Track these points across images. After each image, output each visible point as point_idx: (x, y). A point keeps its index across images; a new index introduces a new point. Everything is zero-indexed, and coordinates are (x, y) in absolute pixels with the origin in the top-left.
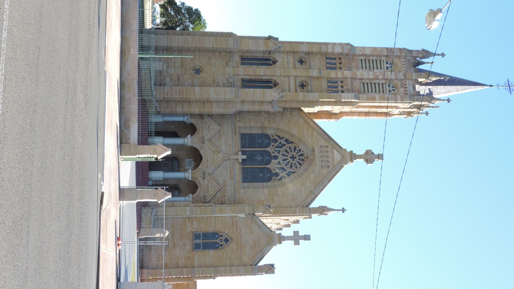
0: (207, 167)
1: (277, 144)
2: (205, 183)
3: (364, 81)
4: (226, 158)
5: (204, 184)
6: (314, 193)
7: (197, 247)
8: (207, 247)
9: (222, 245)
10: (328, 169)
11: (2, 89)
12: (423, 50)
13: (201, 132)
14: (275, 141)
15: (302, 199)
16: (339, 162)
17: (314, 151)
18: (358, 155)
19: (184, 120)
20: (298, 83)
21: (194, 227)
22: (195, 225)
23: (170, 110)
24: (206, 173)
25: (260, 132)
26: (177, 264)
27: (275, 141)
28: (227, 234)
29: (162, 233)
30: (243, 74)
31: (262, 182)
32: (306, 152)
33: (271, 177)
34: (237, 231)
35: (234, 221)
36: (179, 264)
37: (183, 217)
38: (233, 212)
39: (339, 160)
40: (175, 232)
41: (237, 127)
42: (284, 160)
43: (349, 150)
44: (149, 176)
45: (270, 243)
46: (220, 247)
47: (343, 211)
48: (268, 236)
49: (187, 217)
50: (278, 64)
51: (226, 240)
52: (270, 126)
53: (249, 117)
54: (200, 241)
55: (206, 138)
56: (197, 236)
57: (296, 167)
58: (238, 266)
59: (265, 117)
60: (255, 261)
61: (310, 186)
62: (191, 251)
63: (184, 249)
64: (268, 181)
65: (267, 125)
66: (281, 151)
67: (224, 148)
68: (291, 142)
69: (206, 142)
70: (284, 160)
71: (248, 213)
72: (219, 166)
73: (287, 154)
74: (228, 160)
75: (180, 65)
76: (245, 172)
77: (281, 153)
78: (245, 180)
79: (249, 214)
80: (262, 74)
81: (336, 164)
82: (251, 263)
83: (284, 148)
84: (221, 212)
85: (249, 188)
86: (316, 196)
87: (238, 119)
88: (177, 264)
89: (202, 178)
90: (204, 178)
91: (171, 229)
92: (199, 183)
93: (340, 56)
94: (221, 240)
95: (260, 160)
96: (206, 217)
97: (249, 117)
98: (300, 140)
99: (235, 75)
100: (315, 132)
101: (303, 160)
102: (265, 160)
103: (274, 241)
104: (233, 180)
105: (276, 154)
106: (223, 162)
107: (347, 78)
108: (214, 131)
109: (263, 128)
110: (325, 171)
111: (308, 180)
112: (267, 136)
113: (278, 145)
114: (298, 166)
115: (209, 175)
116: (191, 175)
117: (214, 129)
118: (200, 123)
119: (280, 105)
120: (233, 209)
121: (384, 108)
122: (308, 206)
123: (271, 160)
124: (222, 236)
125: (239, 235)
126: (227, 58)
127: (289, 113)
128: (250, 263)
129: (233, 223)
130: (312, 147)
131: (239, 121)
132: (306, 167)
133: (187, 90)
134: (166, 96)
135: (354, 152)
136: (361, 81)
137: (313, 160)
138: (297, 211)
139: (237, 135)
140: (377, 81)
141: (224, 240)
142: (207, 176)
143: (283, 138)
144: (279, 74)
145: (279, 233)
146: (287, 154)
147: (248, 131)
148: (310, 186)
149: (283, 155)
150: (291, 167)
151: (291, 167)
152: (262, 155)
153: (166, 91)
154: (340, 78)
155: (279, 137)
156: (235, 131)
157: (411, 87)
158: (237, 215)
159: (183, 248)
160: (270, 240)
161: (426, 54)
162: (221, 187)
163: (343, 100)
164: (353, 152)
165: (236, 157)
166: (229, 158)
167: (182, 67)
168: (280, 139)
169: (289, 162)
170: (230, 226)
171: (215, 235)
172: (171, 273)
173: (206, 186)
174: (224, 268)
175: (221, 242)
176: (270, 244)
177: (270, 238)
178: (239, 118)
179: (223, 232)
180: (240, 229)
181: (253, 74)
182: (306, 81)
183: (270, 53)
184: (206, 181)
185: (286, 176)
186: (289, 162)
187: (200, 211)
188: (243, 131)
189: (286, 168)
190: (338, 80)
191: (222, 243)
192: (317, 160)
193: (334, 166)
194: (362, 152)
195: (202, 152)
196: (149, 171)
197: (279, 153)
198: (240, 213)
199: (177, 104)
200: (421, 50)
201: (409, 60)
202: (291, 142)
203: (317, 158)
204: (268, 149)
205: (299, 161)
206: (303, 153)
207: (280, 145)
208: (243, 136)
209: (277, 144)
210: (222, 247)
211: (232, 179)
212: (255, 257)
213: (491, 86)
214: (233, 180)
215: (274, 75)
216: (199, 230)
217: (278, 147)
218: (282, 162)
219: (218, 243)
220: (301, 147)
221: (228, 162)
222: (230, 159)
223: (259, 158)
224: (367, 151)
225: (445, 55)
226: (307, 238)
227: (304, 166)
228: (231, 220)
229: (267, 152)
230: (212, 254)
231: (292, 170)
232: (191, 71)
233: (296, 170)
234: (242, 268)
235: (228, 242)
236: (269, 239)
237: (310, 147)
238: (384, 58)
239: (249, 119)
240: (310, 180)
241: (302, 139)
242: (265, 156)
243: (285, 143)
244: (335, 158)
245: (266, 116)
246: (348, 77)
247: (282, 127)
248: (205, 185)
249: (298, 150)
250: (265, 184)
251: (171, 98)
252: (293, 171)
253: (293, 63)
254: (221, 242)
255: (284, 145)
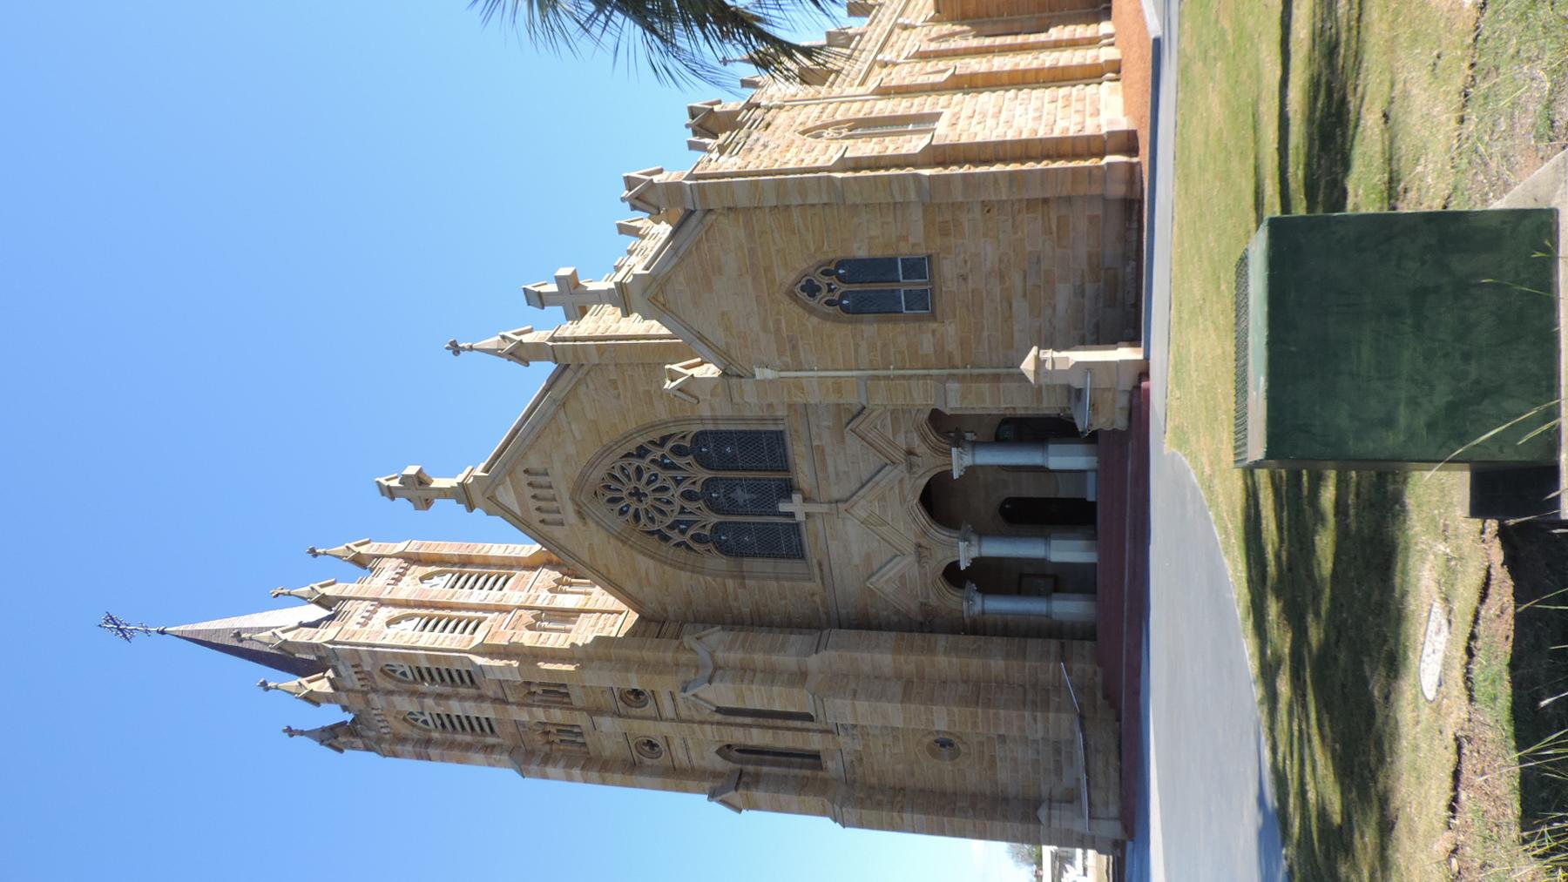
0: (901, 481)
1: (690, 532)
2: (906, 437)
3: (473, 691)
4: (842, 506)
5: (909, 435)
7: (915, 267)
9: (826, 273)
12: (341, 751)
14: (698, 538)
16: (498, 485)
17: (580, 514)
21: (930, 336)
22: (927, 345)
23: (1027, 664)
24: (903, 467)
26: (988, 211)
27: (698, 538)
28: (811, 311)
29: (1047, 372)
30: (811, 734)
32: (601, 509)
34: (778, 322)
38: (798, 385)
39: (501, 488)
41: (819, 581)
42: (664, 489)
44: (1095, 459)
45: (655, 285)
46: (832, 267)
50: (716, 748)
51: (811, 289)
53: (783, 602)
54: (904, 286)
55: (911, 559)
56: (922, 303)
57: (623, 469)
59: (736, 599)
60: (696, 227)
62: (938, 254)
63: (966, 262)
65: (730, 583)
68: (651, 533)
69: (909, 548)
70: (664, 489)
71: (743, 380)
72: (862, 486)
73: (658, 505)
75: (999, 764)
76: (781, 462)
77: (677, 509)
78: (778, 437)
79: (741, 377)
80: (755, 731)
81: (508, 479)
82: (710, 218)
83: (669, 521)
84: (838, 385)
85: (762, 419)
86: (546, 390)
87: (817, 598)
88: (988, 211)
89: (918, 451)
91: (1015, 328)
92: (924, 438)
93: (551, 750)
94: (830, 290)
95: (739, 491)
98: (624, 543)
100: (587, 560)
101: (608, 487)
102: (722, 491)
103: (644, 291)
104: (815, 444)
105: (690, 506)
107: (519, 704)
108: (887, 577)
109: (741, 576)
110: (534, 462)
111: (578, 437)
112: (725, 550)
114: (617, 473)
115: (894, 460)
116: (951, 461)
117: (887, 582)
120: (799, 394)
121: (414, 601)
122: (510, 475)
123: (702, 488)
124: (829, 303)
125: (766, 310)
126: (859, 770)
129: (794, 348)
130: (585, 524)
132: (594, 473)
133: (975, 724)
135: (462, 507)
137: (578, 487)
138: (594, 352)
139: (815, 561)
140: (437, 688)
141: (819, 289)
142: (900, 456)
144: (707, 728)
145: (628, 316)
146: (658, 505)
147: (785, 566)
148: (569, 423)
149: (668, 502)
151: (639, 471)
153: (1040, 725)
154: (539, 706)
155: (689, 548)
156: (821, 570)
159: (969, 263)
160: (657, 295)
161: (331, 737)
162: (850, 426)
163: (515, 664)
167: (993, 760)
169: (649, 482)
170: (801, 338)
171: (858, 307)
172: (1011, 186)
173: (903, 430)
174: (810, 201)
175: (829, 285)
176: (655, 279)
178: (815, 602)
179: (825, 317)
180: (765, 329)
182: (629, 705)
184: (901, 441)
185: (650, 447)
187: (910, 392)
188: (796, 566)
189: (655, 469)
190: (544, 698)
191: (826, 280)
192: (563, 490)
193: (511, 473)
194: (439, 504)
197: (683, 508)
199: (1004, 677)
202: (651, 533)
203: (566, 496)
205: (619, 486)
206: (611, 506)
207: (683, 527)
209: (690, 532)
214: (815, 444)
215: (722, 727)
217: (689, 524)
218: (670, 484)
219: (841, 279)
220: (619, 523)
221: (836, 495)
222: (830, 502)
223: (741, 495)
225: (285, 731)
227: (598, 474)
228: (802, 354)
229: (718, 511)
231: (636, 462)
233: (624, 463)
234: (743, 201)
235: (803, 282)
236: (661, 298)
237: (589, 521)
238: (436, 735)
239: (785, 598)
240: (574, 437)
241: (621, 545)
242: (724, 500)
243: (669, 533)
244: (512, 495)
245: (736, 604)
246: (515, 707)
248: (906, 432)
249: (626, 512)
250: (710, 427)
251: (1024, 704)
252: (631, 460)
255: (671, 527)
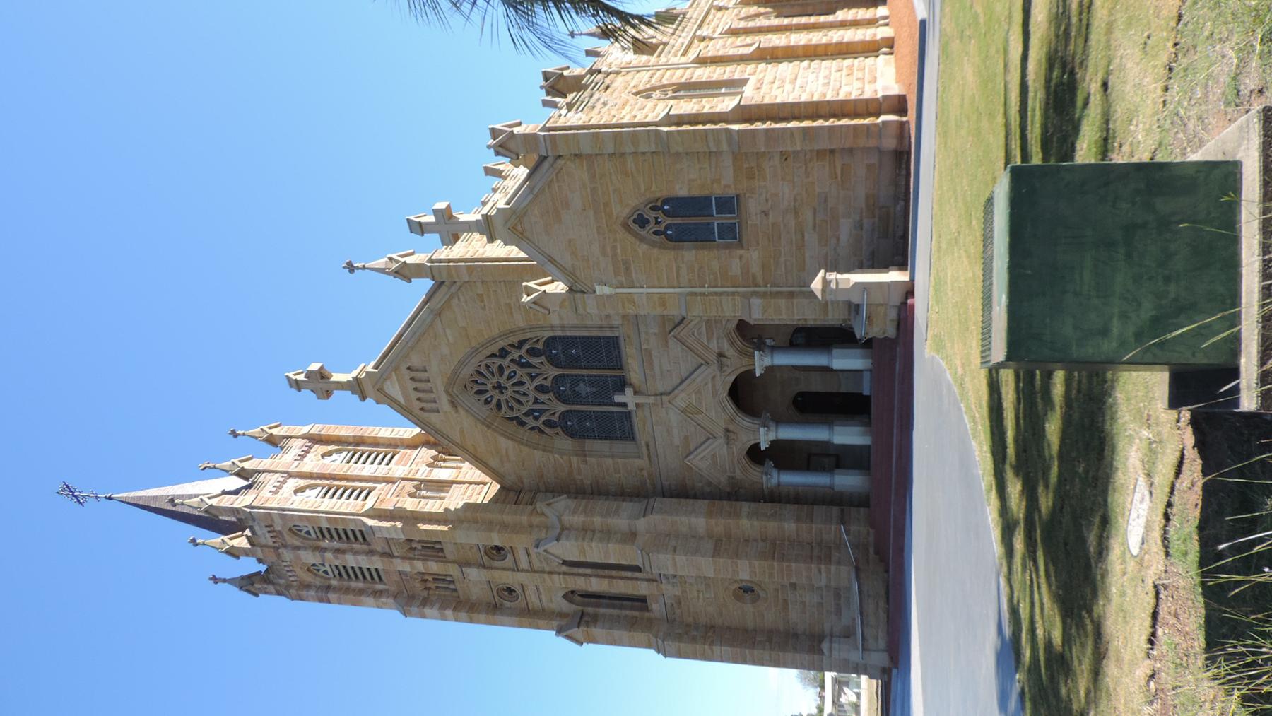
0: (714, 378)
1: (543, 419)
2: (718, 343)
3: (365, 547)
4: (665, 398)
5: (720, 341)
6: (432, 311)
7: (727, 204)
8: (697, 205)
9: (654, 209)
10: (409, 364)
11: (1130, 139)
12: (256, 595)
13: (733, 453)
14: (548, 423)
15: (459, 299)
17: (453, 403)
18: (346, 390)
19: (779, 476)
20: (509, 557)
22: (735, 268)
24: (715, 367)
25: (590, 445)
26: (786, 159)
27: (548, 423)
28: (642, 239)
29: (832, 290)
31: (564, 337)
33: (547, 347)
34: (614, 248)
35: (623, 274)
36: (781, 158)
37: (771, 286)
38: (630, 299)
40: (794, 248)
41: (646, 458)
42: (521, 383)
43: (369, 401)
44: (870, 361)
45: (514, 217)
46: (659, 204)
47: (352, 266)
48: (522, 234)
49: (760, 286)
51: (642, 222)
52: (565, 457)
53: (617, 476)
54: (717, 220)
56: (731, 234)
57: (488, 367)
58: (596, 155)
59: (579, 473)
60: (548, 169)
61: (444, 329)
62: (745, 194)
63: (767, 201)
64: (553, 338)
66: (531, 403)
67: (674, 417)
68: (511, 419)
69: (720, 432)
70: (521, 383)
71: (585, 295)
73: (517, 396)
74: (661, 394)
76: (616, 362)
77: (532, 400)
78: (613, 343)
80: (594, 580)
82: (561, 162)
83: (525, 409)
84: (663, 301)
86: (425, 302)
87: (645, 473)
88: (786, 159)
90: (721, 355)
91: (807, 255)
92: (732, 344)
94: (657, 223)
95: (582, 385)
96: (704, 287)
97: (617, 476)
98: (488, 427)
99: (656, 581)
105: (542, 397)
106: (673, 390)
108: (702, 455)
109: (583, 455)
110: (416, 360)
112: (570, 433)
113: (541, 414)
118: (738, 471)
119: (542, 518)
122: (439, 285)
124: (656, 233)
126: (678, 612)
127: (526, 481)
128: (563, 162)
129: (627, 269)
130: (457, 411)
131: (642, 470)
134: (823, 567)
136: (372, 547)
137: (451, 382)
139: (643, 443)
140: (336, 544)
141: (648, 222)
143: (532, 429)
145: (493, 242)
146: (517, 396)
148: (444, 329)
150: (501, 368)
151: (501, 368)
152: (577, 394)
154: (418, 559)
155: (541, 431)
156: (648, 450)
157: (259, 532)
158: (618, 290)
159: (770, 202)
161: (249, 584)
163: (399, 525)
164: (358, 399)
165: (641, 399)
166: (659, 397)
168: (537, 427)
169: (509, 378)
171: (679, 237)
175: (656, 218)
177: (516, 230)
178: (643, 476)
180: (604, 253)
181: (614, 580)
182: (491, 558)
183: (580, 614)
184: (714, 345)
185: (510, 349)
186: (509, 378)
191: (654, 214)
192: (439, 384)
193: (396, 369)
195: (730, 407)
196: (869, 446)
197: (536, 399)
198: (609, 297)
200: (260, 595)
201: (280, 577)
204: (563, 408)
205: (484, 381)
207: (536, 414)
208: (629, 436)
209: (543, 419)
210: (653, 204)
211: (646, 350)
212: (552, 179)
213: (110, 498)
214: (643, 347)
216: (724, 251)
217: (541, 412)
218: (526, 379)
220: (484, 411)
221: (661, 389)
222: (656, 395)
223: (583, 389)
224: (328, 398)
225: (211, 579)
226: (419, 228)
227: (468, 370)
228: (634, 275)
230: (681, 188)
231: (499, 361)
232: (762, 594)
233: (489, 362)
236: (519, 228)
238: (334, 582)
243: (525, 419)
244: (397, 387)
245: (580, 478)
247: (538, 454)
248: (718, 339)
250: (559, 333)
253: (527, 593)
254: (656, 218)
255: (526, 414)
